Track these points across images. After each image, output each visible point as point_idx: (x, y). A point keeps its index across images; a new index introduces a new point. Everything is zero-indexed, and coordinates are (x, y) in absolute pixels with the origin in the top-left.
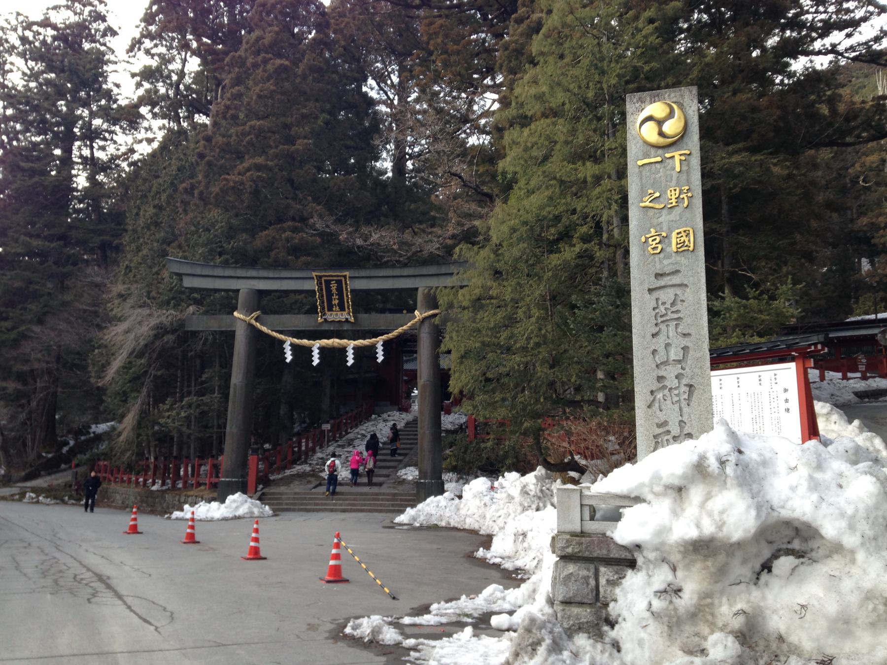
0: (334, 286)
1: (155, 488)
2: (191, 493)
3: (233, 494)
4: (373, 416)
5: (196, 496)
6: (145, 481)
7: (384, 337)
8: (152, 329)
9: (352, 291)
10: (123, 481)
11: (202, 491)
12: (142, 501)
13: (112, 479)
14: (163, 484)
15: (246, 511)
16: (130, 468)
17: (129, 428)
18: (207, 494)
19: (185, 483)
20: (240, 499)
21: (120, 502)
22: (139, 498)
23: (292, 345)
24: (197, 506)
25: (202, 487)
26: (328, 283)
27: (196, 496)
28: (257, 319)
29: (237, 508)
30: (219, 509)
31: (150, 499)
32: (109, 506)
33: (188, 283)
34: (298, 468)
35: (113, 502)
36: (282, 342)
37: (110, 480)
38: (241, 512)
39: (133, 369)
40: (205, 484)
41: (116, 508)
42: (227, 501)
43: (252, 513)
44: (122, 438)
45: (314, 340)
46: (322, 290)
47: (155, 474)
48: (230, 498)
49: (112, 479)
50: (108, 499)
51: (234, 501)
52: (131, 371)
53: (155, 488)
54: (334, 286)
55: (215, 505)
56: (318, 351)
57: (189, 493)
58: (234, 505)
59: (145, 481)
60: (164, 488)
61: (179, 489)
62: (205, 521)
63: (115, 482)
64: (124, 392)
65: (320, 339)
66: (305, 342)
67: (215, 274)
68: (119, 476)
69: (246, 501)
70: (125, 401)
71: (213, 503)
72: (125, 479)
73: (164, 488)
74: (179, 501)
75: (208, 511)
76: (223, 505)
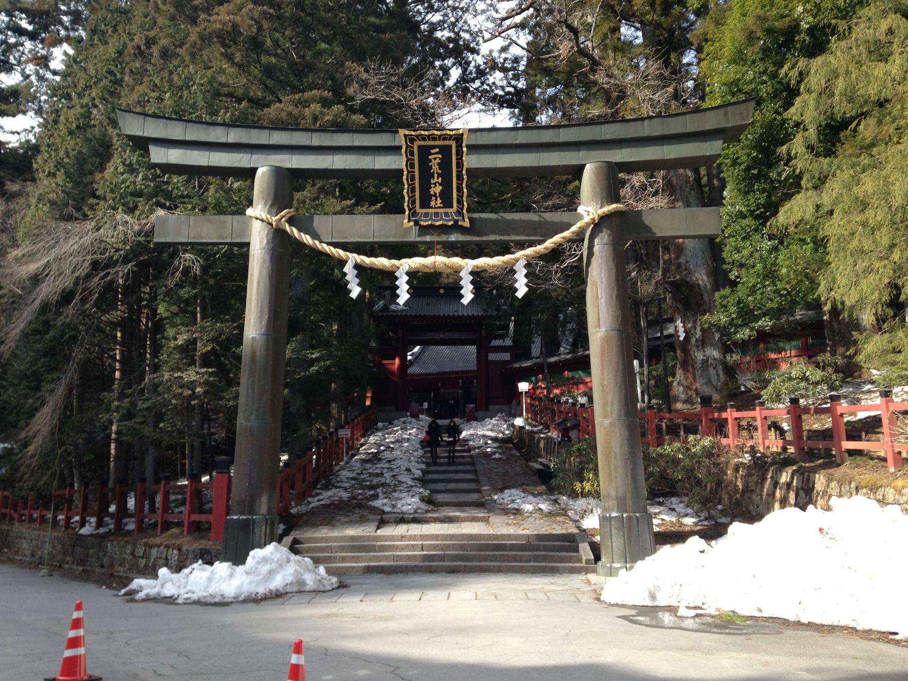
0: (435, 160)
1: (85, 531)
2: (158, 540)
3: (262, 546)
4: (380, 424)
5: (167, 547)
6: (68, 519)
7: (529, 251)
8: (83, 249)
9: (468, 170)
10: (31, 520)
11: (177, 536)
12: (65, 553)
13: (16, 516)
14: (100, 524)
15: (289, 579)
16: (44, 500)
17: (45, 430)
18: (190, 544)
19: (140, 523)
20: (277, 556)
21: (28, 553)
22: (59, 547)
23: (357, 266)
24: (186, 571)
25: (175, 530)
26: (425, 152)
27: (167, 547)
28: (291, 221)
29: (271, 573)
30: (231, 576)
31: (78, 549)
32: (11, 561)
33: (158, 155)
34: (326, 496)
35: (17, 552)
36: (342, 263)
37: (12, 519)
38: (278, 582)
39: (52, 333)
40: (179, 524)
41: (22, 564)
42: (249, 560)
43: (302, 583)
44: (31, 448)
45: (399, 259)
46: (412, 166)
47: (84, 509)
48: (256, 554)
49: (16, 516)
50: (9, 547)
51: (265, 560)
52: (48, 337)
53: (85, 531)
54: (435, 160)
55: (222, 568)
56: (406, 278)
57: (152, 541)
58: (265, 569)
59: (68, 519)
60: (102, 530)
61: (129, 533)
62: (206, 604)
63: (20, 521)
64: (35, 373)
65: (410, 257)
66: (383, 262)
67: (211, 139)
68: (26, 512)
69: (288, 561)
70: (38, 388)
71: (217, 564)
72: (35, 516)
73: (102, 530)
74: (132, 553)
75: (210, 580)
76: (241, 569)
